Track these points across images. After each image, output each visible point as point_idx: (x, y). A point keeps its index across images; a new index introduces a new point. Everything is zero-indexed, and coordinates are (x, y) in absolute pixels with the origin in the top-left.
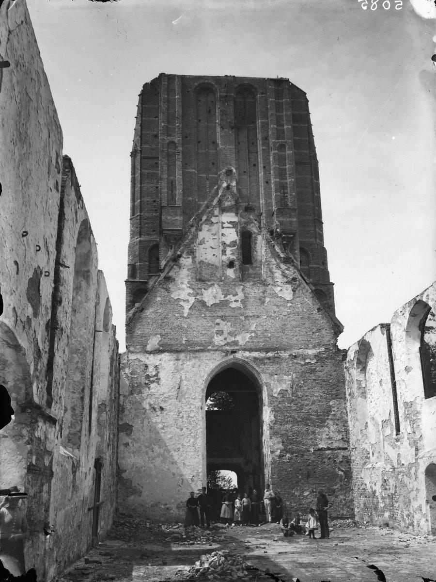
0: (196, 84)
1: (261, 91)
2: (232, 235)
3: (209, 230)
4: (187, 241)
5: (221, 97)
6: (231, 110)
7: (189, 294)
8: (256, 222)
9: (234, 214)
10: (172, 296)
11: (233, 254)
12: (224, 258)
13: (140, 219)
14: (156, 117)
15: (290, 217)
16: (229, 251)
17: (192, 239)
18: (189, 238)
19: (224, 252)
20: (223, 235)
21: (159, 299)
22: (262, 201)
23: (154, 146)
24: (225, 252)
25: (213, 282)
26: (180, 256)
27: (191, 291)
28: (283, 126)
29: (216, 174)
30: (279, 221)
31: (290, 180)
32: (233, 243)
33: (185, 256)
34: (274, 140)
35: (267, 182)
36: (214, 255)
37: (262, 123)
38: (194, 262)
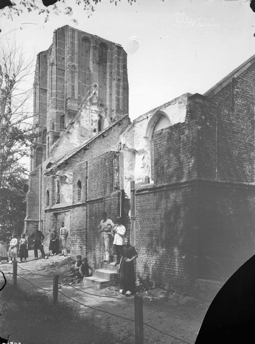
0: (83, 36)
1: (110, 48)
2: (96, 117)
3: (85, 112)
4: (77, 116)
5: (93, 46)
6: (97, 54)
7: (77, 142)
8: (104, 112)
9: (97, 107)
10: (70, 141)
11: (96, 126)
12: (92, 127)
13: (56, 100)
14: (64, 48)
15: (120, 114)
16: (94, 123)
17: (79, 115)
18: (78, 115)
19: (92, 124)
20: (92, 116)
21: (64, 142)
22: (76, 85)
23: (63, 64)
24: (93, 124)
25: (87, 138)
26: (74, 123)
27: (78, 140)
28: (120, 70)
29: (89, 84)
30: (117, 115)
31: (121, 97)
32: (95, 121)
33: (76, 123)
34: (116, 76)
35: (111, 95)
36: (87, 124)
37: (110, 65)
38: (80, 127)
